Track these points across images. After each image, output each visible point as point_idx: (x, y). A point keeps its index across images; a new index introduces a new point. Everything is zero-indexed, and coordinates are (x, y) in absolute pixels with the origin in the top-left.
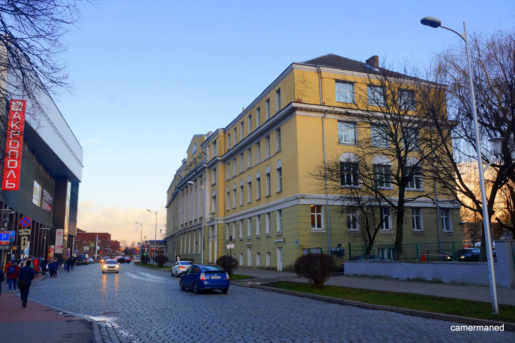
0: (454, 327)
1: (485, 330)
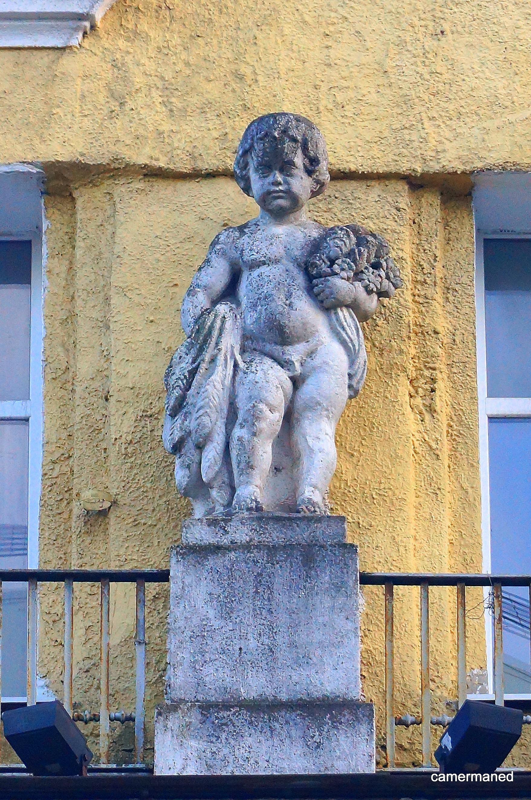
0: (437, 775)
1: (484, 780)
